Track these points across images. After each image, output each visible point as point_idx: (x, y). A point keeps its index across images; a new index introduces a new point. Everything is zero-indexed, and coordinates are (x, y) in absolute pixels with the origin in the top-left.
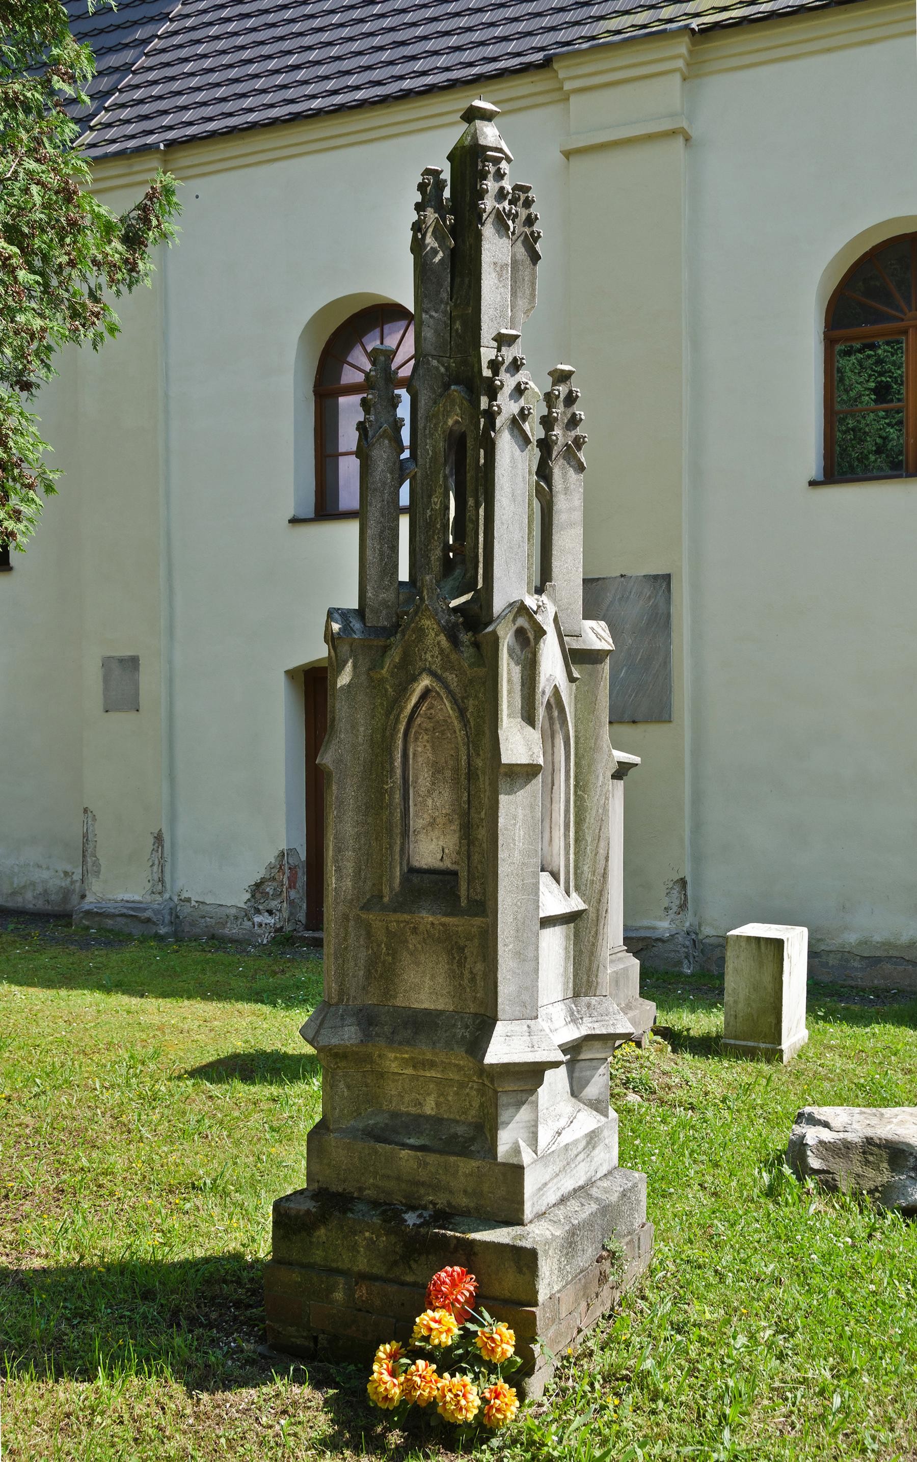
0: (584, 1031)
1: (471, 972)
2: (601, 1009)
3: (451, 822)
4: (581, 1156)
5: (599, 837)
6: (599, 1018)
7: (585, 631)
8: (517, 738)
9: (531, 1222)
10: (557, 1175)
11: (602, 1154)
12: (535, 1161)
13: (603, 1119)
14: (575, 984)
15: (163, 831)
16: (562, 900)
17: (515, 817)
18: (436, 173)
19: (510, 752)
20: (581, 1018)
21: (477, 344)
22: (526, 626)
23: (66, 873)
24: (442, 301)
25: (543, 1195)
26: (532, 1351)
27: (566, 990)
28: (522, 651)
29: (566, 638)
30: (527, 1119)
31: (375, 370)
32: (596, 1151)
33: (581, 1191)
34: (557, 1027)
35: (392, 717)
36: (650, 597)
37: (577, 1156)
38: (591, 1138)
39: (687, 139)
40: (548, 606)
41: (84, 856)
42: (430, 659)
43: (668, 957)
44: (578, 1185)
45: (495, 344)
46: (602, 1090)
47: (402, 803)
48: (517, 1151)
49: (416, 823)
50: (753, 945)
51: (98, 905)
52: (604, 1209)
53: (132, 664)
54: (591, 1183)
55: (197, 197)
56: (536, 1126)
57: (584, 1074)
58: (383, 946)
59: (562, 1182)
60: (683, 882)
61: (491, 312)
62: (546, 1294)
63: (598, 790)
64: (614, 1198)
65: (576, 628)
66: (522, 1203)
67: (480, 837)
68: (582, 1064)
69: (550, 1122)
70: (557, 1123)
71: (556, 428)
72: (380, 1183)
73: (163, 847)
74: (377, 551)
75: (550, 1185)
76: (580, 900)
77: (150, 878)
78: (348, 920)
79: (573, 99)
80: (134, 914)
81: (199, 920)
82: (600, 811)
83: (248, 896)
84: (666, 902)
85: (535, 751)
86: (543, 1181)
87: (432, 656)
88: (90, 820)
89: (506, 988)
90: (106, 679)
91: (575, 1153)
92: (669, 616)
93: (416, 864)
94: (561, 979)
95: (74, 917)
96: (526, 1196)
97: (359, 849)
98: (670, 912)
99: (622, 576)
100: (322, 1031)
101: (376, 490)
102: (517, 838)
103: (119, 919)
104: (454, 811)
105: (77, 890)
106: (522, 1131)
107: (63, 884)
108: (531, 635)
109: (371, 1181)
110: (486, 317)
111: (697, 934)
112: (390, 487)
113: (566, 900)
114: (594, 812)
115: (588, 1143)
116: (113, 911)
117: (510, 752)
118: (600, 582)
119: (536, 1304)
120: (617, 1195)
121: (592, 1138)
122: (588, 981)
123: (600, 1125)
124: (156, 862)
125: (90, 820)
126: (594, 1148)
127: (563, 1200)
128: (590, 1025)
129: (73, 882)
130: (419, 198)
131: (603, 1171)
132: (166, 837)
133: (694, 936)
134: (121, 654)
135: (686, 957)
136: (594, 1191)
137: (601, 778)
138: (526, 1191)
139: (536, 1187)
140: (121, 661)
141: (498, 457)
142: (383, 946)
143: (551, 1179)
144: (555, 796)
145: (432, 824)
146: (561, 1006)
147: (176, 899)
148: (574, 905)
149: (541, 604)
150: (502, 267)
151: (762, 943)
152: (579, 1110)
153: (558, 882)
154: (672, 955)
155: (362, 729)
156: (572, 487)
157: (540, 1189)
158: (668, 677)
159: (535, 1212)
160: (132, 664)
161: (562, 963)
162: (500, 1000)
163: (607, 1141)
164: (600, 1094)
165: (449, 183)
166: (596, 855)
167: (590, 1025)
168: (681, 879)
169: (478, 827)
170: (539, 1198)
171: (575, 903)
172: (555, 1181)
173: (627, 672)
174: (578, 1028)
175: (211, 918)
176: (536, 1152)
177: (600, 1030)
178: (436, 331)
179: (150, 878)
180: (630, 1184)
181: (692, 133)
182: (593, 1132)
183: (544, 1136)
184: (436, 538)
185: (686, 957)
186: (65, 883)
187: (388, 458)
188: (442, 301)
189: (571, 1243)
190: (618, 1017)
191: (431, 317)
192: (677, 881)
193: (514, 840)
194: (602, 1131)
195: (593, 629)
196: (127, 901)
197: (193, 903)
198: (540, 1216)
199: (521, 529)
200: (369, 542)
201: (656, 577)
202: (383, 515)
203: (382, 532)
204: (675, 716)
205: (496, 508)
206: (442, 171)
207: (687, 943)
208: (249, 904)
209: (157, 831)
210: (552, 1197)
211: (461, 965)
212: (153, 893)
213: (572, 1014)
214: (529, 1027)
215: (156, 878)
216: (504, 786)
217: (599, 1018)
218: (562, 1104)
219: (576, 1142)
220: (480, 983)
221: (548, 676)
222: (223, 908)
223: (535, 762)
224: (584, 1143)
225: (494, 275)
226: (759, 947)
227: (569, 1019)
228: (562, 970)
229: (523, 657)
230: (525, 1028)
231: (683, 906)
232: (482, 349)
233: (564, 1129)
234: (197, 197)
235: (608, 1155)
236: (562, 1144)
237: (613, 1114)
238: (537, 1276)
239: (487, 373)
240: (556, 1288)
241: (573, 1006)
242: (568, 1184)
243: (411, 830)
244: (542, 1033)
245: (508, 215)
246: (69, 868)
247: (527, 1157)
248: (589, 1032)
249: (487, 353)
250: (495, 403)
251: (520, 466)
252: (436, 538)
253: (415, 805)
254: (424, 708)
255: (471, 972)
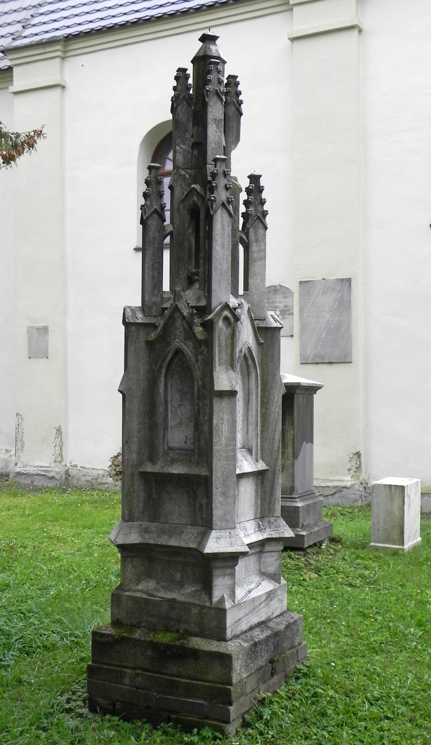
0: (265, 536)
1: (200, 504)
2: (276, 524)
3: (190, 421)
4: (263, 605)
5: (275, 429)
6: (275, 529)
7: (267, 317)
8: (224, 376)
9: (230, 640)
10: (247, 614)
11: (276, 604)
12: (233, 607)
13: (277, 585)
14: (261, 510)
15: (62, 426)
16: (253, 464)
17: (222, 419)
18: (185, 70)
19: (220, 384)
20: (265, 529)
21: (205, 163)
22: (229, 315)
23: (7, 451)
24: (187, 139)
25: (238, 625)
26: (229, 710)
27: (256, 513)
28: (227, 329)
29: (256, 322)
30: (229, 583)
31: (150, 177)
32: (273, 602)
33: (262, 624)
34: (249, 534)
35: (158, 365)
36: (339, 291)
37: (260, 604)
38: (269, 595)
39: (360, 31)
40: (244, 304)
41: (16, 441)
42: (179, 334)
43: (350, 497)
44: (261, 620)
45: (214, 163)
46: (277, 568)
47: (164, 412)
48: (222, 600)
49: (171, 422)
50: (388, 489)
51: (24, 469)
52: (276, 634)
53: (45, 330)
54: (269, 620)
55: (83, 66)
56: (234, 587)
57: (267, 559)
58: (153, 489)
59: (250, 619)
60: (358, 454)
61: (213, 145)
62: (237, 679)
63: (275, 404)
64: (282, 627)
65: (262, 315)
66: (225, 629)
67: (205, 430)
68: (266, 554)
69: (245, 586)
70: (249, 586)
71: (251, 207)
72: (149, 619)
73: (61, 436)
74: (151, 275)
75: (243, 620)
76: (264, 464)
77: (54, 453)
78: (134, 476)
79: (295, 9)
80: (44, 474)
81: (82, 477)
82: (276, 415)
83: (110, 463)
84: (349, 466)
85: (234, 383)
86: (238, 618)
87: (180, 332)
88: (20, 420)
89: (217, 513)
90: (30, 339)
91: (259, 602)
92: (350, 302)
93: (171, 445)
94: (253, 508)
95: (10, 476)
96: (228, 625)
97: (140, 437)
98: (351, 471)
99: (323, 279)
100: (119, 536)
101: (150, 242)
102: (223, 431)
103: (36, 477)
104: (192, 416)
105: (13, 460)
106: (226, 590)
107: (5, 457)
108: (232, 319)
109: (145, 618)
110: (210, 148)
111: (367, 484)
112: (158, 240)
113: (255, 464)
114: (272, 416)
115: (267, 598)
116: (33, 472)
117: (220, 384)
118: (311, 283)
119: (231, 684)
120: (283, 626)
121: (270, 595)
122: (269, 509)
123: (275, 587)
124: (58, 444)
125: (20, 420)
126: (271, 600)
127: (251, 628)
128: (269, 533)
129: (10, 456)
130: (175, 84)
131: (278, 613)
132: (63, 430)
133: (365, 485)
134: (38, 325)
135: (360, 497)
136: (271, 624)
137: (276, 397)
138: (227, 622)
139: (234, 621)
140: (38, 329)
141: (214, 225)
142: (153, 489)
143: (243, 617)
144: (250, 407)
145: (181, 423)
146: (253, 522)
147: (69, 465)
148: (260, 467)
149: (240, 303)
150: (218, 121)
151: (393, 488)
152: (264, 580)
153: (251, 454)
154: (352, 496)
155: (142, 372)
156: (260, 238)
157: (236, 622)
158: (349, 337)
159: (233, 635)
160: (45, 330)
161: (254, 499)
162: (214, 519)
163: (280, 597)
164: (276, 571)
165: (191, 76)
166: (273, 439)
167: (269, 533)
168: (358, 452)
169: (204, 425)
170: (236, 627)
171: (262, 466)
172: (246, 618)
173: (326, 334)
174: (262, 534)
175: (89, 476)
176: (234, 602)
177: (275, 535)
178: (184, 156)
179: (54, 453)
180: (292, 621)
181: (363, 27)
182: (271, 591)
183: (240, 593)
184: (184, 267)
185: (360, 497)
186: (6, 457)
187: (157, 225)
188: (187, 139)
189: (254, 652)
190: (286, 528)
191: (181, 148)
192: (355, 454)
193: (222, 432)
194: (276, 591)
195: (272, 316)
196: (41, 467)
197: (79, 468)
198: (236, 637)
199: (227, 263)
200: (146, 270)
201: (342, 280)
202: (154, 256)
203: (153, 265)
204: (354, 360)
205: (213, 252)
206: (187, 69)
207: (361, 489)
208: (111, 468)
209: (58, 427)
210: (244, 626)
211: (195, 500)
212: (55, 462)
213: (259, 526)
214: (230, 533)
215: (58, 453)
216: (216, 403)
217: (275, 529)
218: (253, 576)
219: (260, 596)
220: (204, 509)
221: (244, 342)
222: (95, 470)
223: (233, 390)
224: (264, 598)
225: (214, 125)
226: (391, 491)
227: (257, 529)
228: (253, 502)
229: (227, 333)
230: (228, 534)
231: (359, 468)
232: (207, 165)
233: (253, 589)
234: (83, 66)
235: (280, 605)
236: (251, 598)
237: (283, 582)
238: (232, 669)
239: (209, 178)
240: (244, 676)
241: (260, 522)
242: (255, 620)
243: (169, 426)
244: (238, 536)
245: (222, 93)
246: (8, 448)
247: (228, 604)
248: (269, 537)
249: (210, 168)
250: (212, 195)
251: (226, 229)
252: (184, 267)
253: (171, 413)
254: (176, 360)
255: (200, 504)
